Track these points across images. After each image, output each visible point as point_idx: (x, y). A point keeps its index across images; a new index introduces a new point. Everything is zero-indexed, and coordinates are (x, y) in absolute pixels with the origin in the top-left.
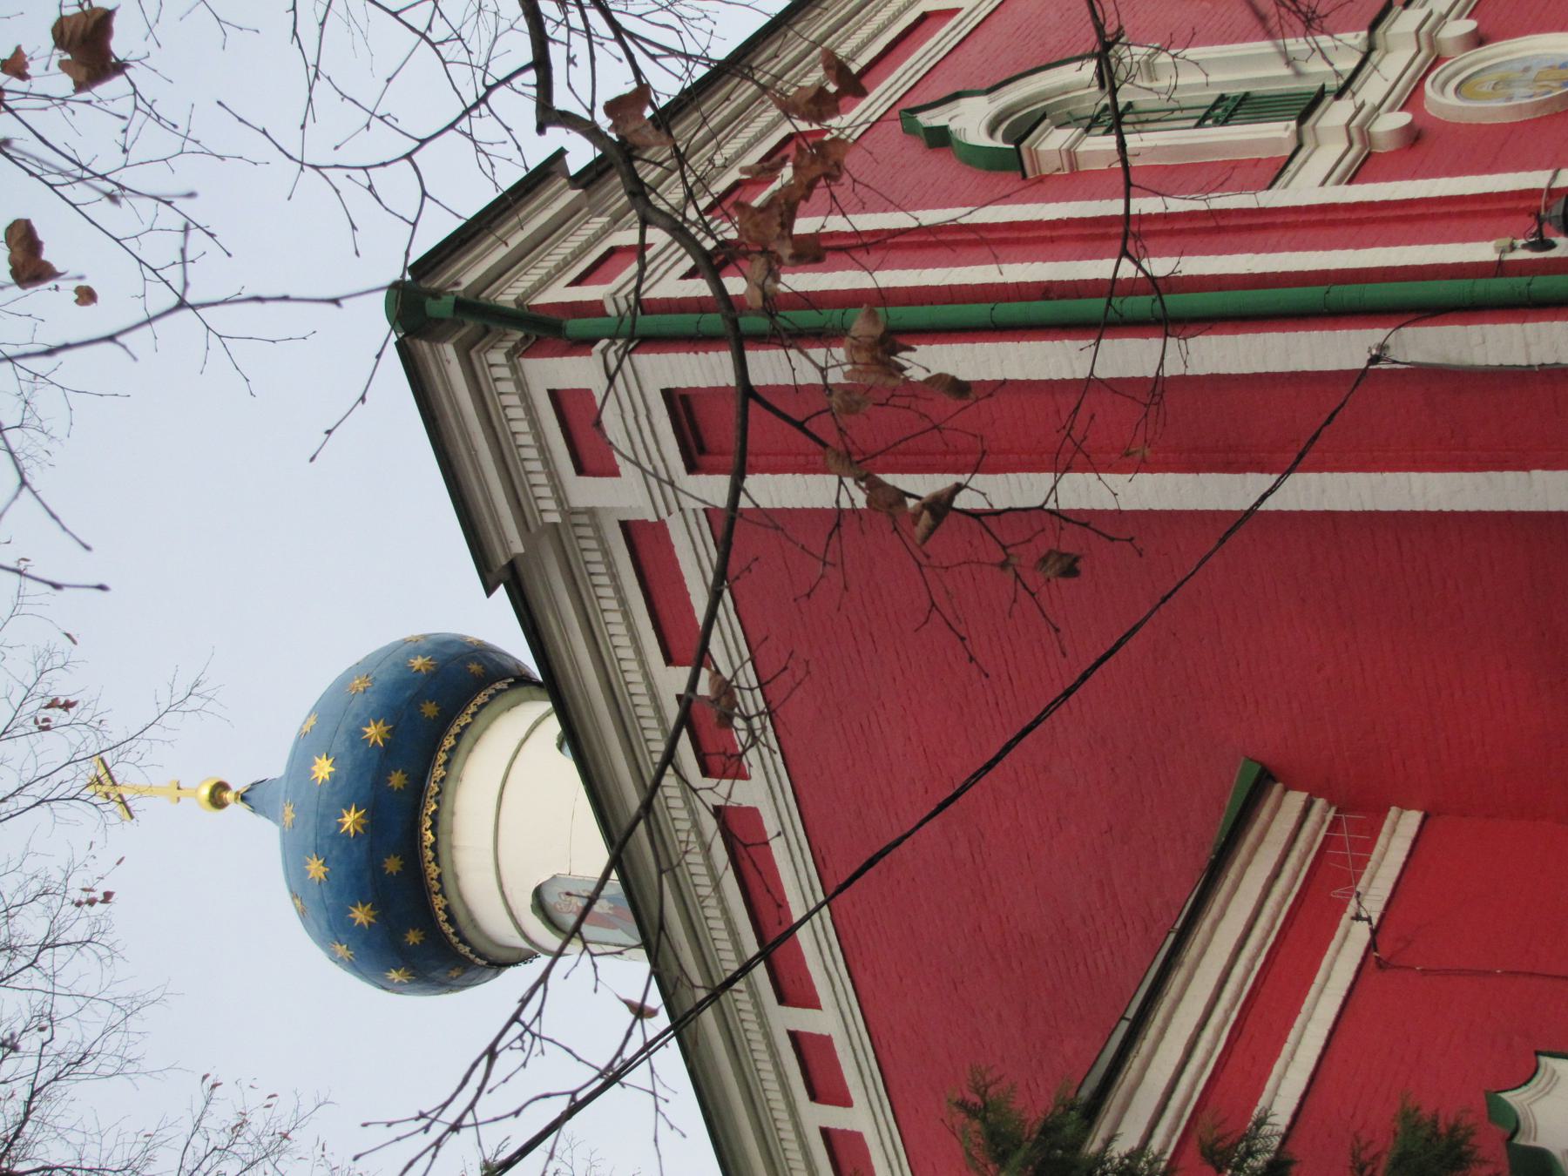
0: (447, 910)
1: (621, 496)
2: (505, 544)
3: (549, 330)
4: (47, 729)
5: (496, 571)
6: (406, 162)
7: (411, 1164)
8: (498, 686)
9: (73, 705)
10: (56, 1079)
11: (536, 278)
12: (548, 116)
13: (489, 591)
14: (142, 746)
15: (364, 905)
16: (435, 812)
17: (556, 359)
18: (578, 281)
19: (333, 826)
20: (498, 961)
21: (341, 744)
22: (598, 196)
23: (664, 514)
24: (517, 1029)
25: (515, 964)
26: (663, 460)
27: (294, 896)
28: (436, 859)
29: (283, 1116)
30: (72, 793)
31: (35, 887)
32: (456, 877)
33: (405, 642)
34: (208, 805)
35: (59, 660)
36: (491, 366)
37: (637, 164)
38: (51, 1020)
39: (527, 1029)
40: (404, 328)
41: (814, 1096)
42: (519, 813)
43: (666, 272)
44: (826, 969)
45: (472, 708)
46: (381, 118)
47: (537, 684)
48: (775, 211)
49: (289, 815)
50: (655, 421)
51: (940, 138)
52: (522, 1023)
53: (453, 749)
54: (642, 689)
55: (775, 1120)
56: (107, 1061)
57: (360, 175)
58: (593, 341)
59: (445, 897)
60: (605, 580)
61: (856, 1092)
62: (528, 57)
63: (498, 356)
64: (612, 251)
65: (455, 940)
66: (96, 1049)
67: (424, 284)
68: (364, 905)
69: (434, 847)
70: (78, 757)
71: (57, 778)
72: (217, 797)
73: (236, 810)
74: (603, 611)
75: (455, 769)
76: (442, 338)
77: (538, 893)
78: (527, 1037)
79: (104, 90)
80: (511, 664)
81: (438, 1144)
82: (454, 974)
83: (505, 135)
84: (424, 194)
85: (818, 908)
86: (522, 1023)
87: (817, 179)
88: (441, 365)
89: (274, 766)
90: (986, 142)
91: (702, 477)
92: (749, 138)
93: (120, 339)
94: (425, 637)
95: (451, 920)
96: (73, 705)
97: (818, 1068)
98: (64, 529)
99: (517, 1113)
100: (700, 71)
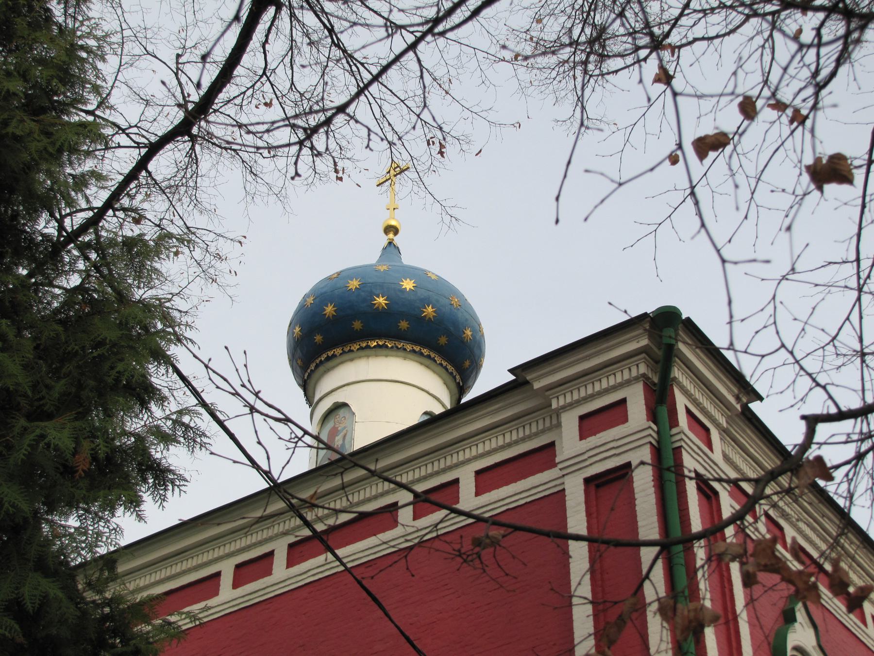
0: (334, 356)
1: (569, 441)
2: (539, 378)
3: (660, 398)
4: (429, 144)
5: (523, 374)
6: (779, 344)
7: (225, 380)
8: (458, 377)
9: (443, 156)
10: (243, 161)
11: (689, 388)
12: (812, 421)
13: (511, 371)
14: (422, 194)
15: (335, 311)
16: (387, 347)
17: (643, 402)
18: (689, 412)
19: (377, 292)
20: (307, 385)
21: (422, 293)
22: (737, 420)
23: (560, 466)
24: (300, 433)
25: (306, 395)
26: (591, 465)
27: (339, 274)
28: (361, 348)
29: (226, 279)
30: (395, 159)
31: (344, 143)
32: (352, 360)
33: (479, 325)
34: (386, 225)
35: (465, 147)
36: (637, 365)
37: (789, 474)
38: (274, 156)
39: (300, 439)
40: (655, 317)
41: (238, 567)
42: (390, 393)
43: (698, 461)
44: (309, 570)
45: (444, 364)
46: (803, 329)
47: (460, 399)
48: (773, 561)
49: (382, 268)
50: (613, 459)
51: (789, 618)
52: (303, 436)
53: (422, 354)
54: (461, 458)
55: (224, 545)
56: (253, 186)
57: (772, 320)
58: (655, 422)
59: (341, 354)
60: (521, 435)
61: (241, 591)
62: (844, 409)
63: (643, 369)
64: (707, 430)
65: (318, 361)
66: (259, 180)
67: (680, 326)
68: (335, 311)
69: (368, 347)
70: (415, 161)
71: (403, 150)
72: (391, 230)
73: (384, 240)
74: (504, 435)
75: (410, 356)
76: (650, 338)
77: (344, 405)
78: (296, 439)
79: (806, 178)
80: (470, 383)
81: (236, 394)
82: (299, 362)
83: (799, 397)
84: (763, 356)
85: (343, 564)
86: (303, 436)
87: (794, 585)
88: (637, 338)
89: (408, 258)
90: (790, 645)
91: (582, 487)
92: (802, 532)
93: (703, 231)
94: (483, 335)
95: (328, 359)
96: (443, 156)
97: (253, 569)
98: (596, 207)
99: (259, 443)
100: (841, 502)
